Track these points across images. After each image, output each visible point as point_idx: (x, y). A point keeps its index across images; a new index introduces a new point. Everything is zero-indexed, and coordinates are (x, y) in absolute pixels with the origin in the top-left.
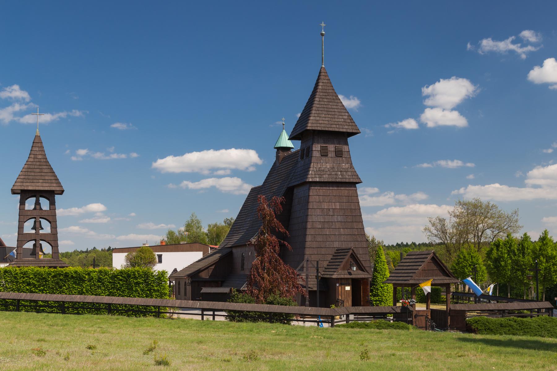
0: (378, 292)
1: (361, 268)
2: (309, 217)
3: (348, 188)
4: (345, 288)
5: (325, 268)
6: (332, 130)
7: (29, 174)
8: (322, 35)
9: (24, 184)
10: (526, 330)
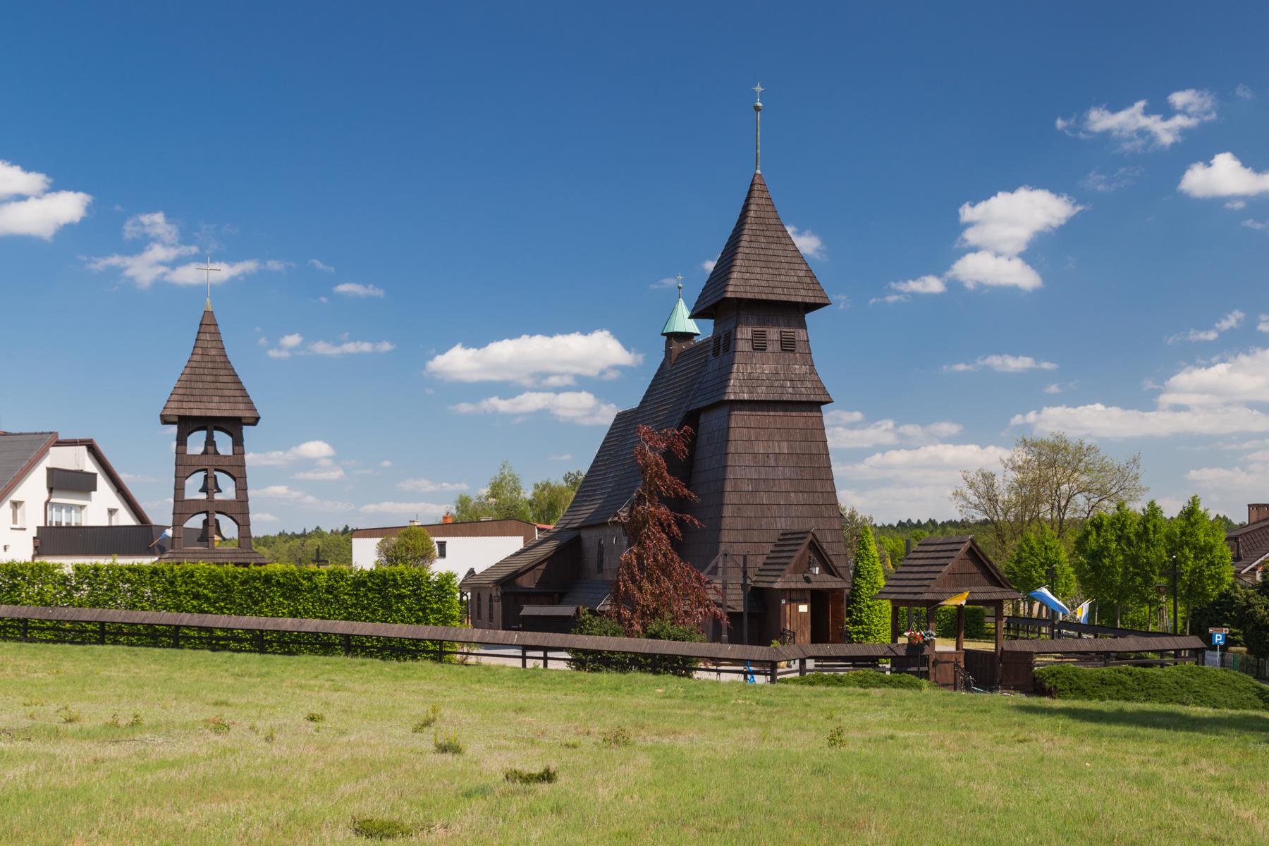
1: (828, 568)
5: (760, 570)
7: (193, 384)
8: (757, 109)
9: (185, 405)
10: (1151, 692)
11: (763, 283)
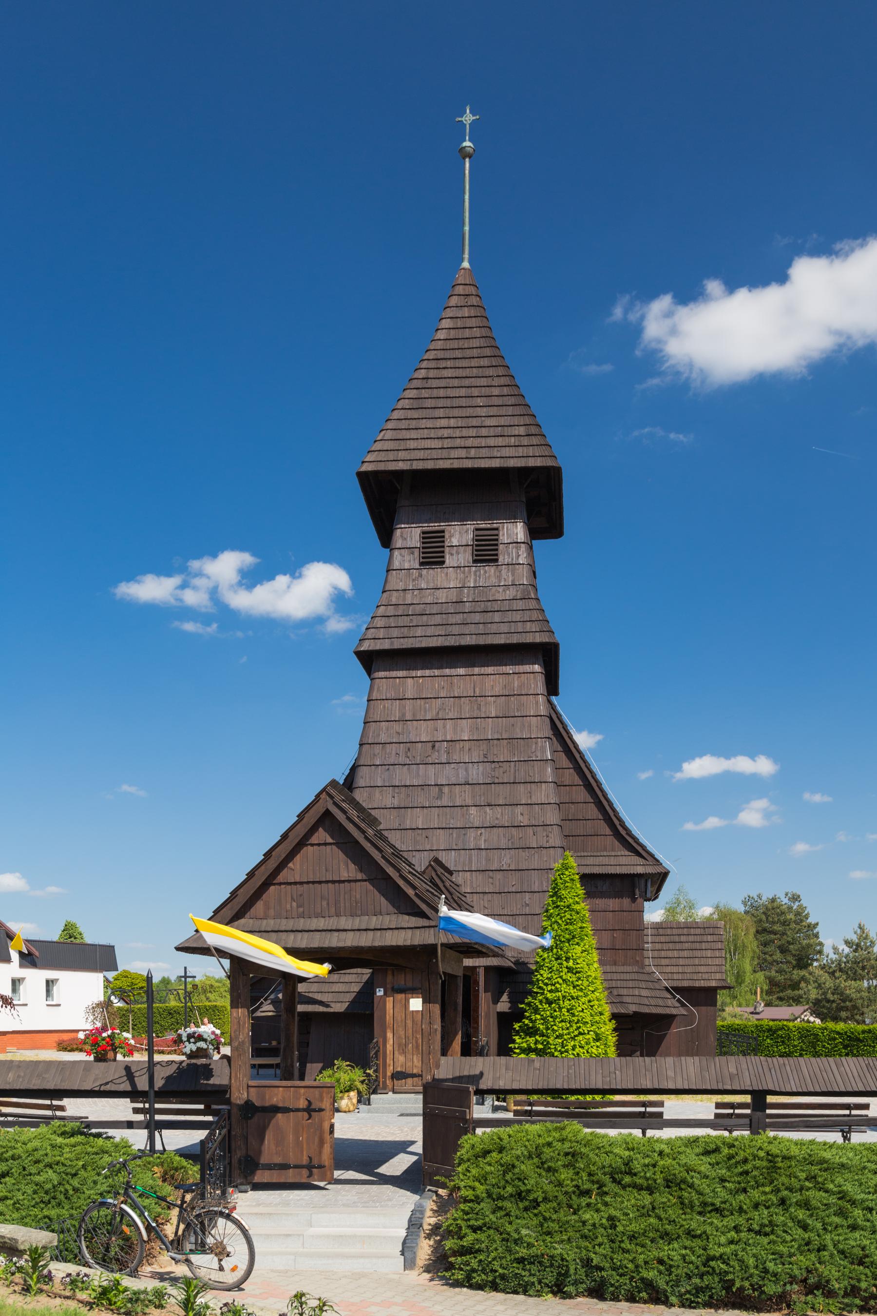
3: (509, 669)
4: (406, 1005)
6: (449, 466)
8: (464, 154)
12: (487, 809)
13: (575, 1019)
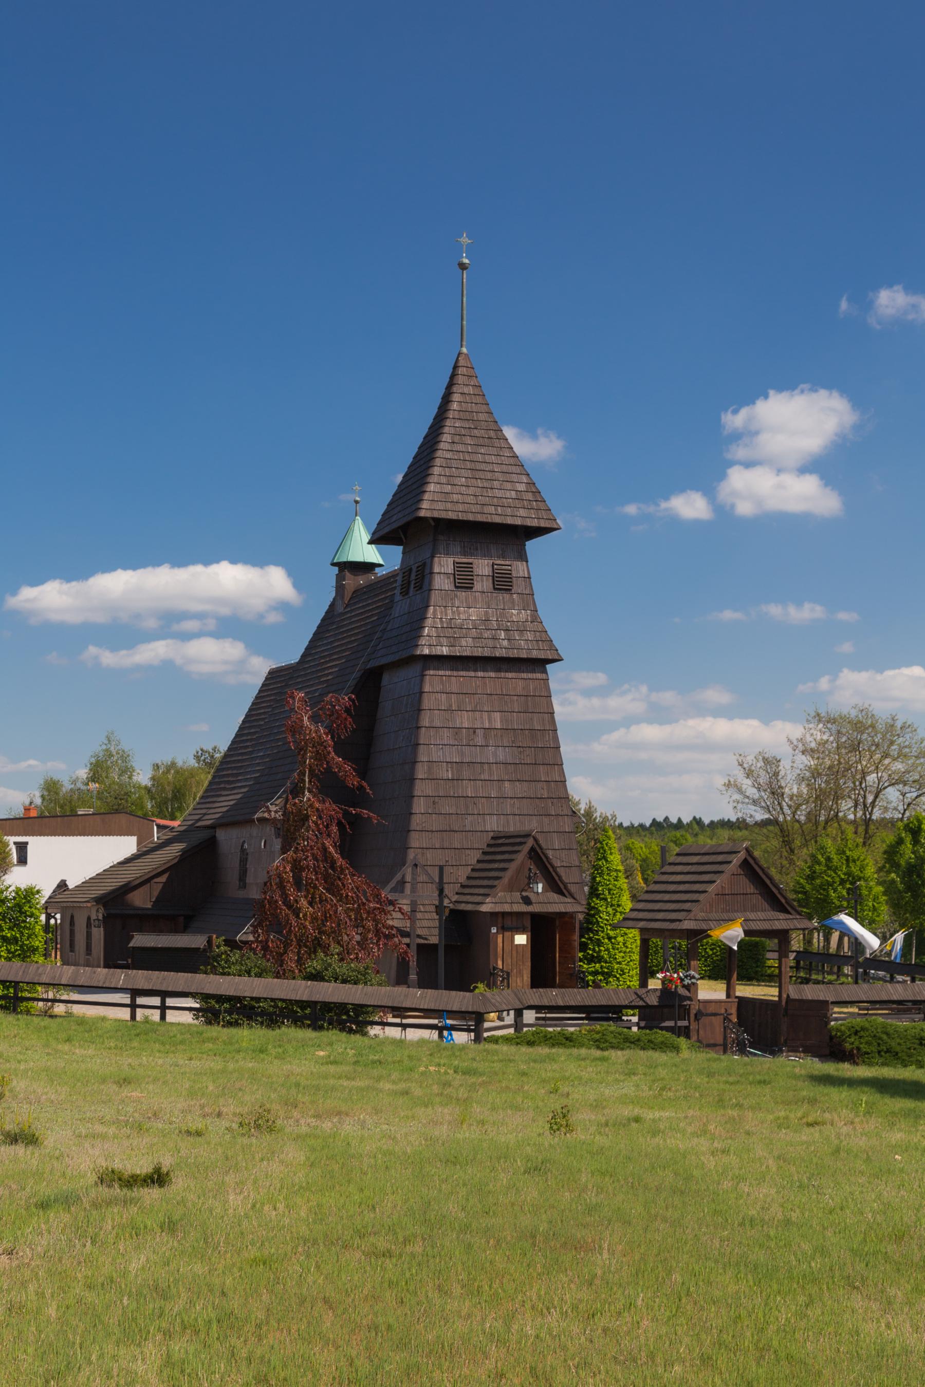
0: (600, 951)
1: (556, 885)
2: (422, 749)
3: (524, 675)
4: (513, 940)
8: (463, 267)
11: (470, 499)
12: (517, 783)
13: (628, 950)
